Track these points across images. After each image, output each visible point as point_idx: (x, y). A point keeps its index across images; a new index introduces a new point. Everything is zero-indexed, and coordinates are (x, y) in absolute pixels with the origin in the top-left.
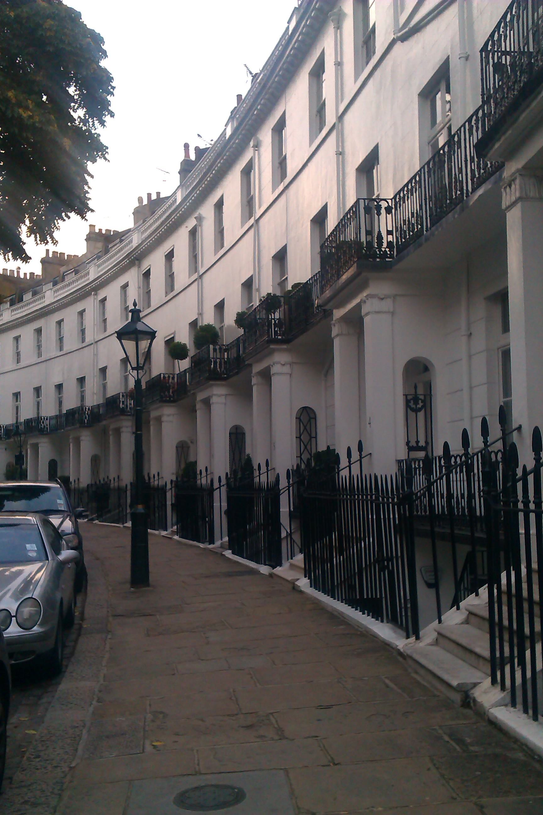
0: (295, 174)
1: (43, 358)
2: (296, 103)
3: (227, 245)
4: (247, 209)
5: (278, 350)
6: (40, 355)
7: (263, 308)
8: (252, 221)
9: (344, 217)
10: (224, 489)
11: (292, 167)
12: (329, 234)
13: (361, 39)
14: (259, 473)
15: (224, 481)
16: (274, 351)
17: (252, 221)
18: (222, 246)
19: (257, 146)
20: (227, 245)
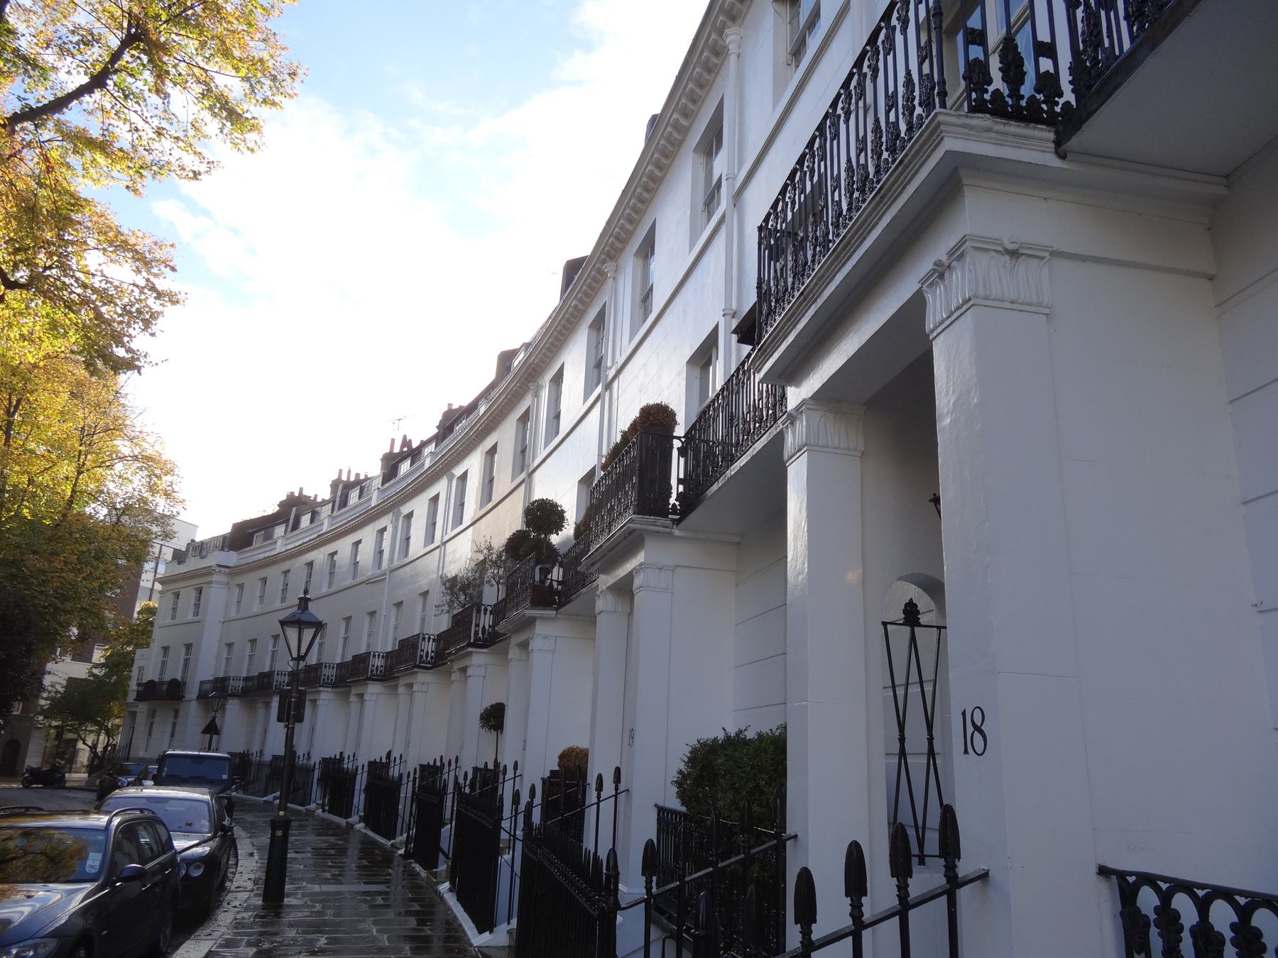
0: (666, 314)
1: (177, 621)
2: (574, 361)
3: (495, 499)
4: (519, 458)
5: (542, 618)
6: (173, 617)
7: (110, 873)
8: (523, 475)
9: (737, 371)
10: (365, 775)
11: (565, 424)
12: (718, 388)
13: (593, 363)
14: (599, 796)
15: (366, 768)
16: (470, 654)
17: (523, 475)
18: (490, 500)
19: (537, 395)
20: (495, 499)
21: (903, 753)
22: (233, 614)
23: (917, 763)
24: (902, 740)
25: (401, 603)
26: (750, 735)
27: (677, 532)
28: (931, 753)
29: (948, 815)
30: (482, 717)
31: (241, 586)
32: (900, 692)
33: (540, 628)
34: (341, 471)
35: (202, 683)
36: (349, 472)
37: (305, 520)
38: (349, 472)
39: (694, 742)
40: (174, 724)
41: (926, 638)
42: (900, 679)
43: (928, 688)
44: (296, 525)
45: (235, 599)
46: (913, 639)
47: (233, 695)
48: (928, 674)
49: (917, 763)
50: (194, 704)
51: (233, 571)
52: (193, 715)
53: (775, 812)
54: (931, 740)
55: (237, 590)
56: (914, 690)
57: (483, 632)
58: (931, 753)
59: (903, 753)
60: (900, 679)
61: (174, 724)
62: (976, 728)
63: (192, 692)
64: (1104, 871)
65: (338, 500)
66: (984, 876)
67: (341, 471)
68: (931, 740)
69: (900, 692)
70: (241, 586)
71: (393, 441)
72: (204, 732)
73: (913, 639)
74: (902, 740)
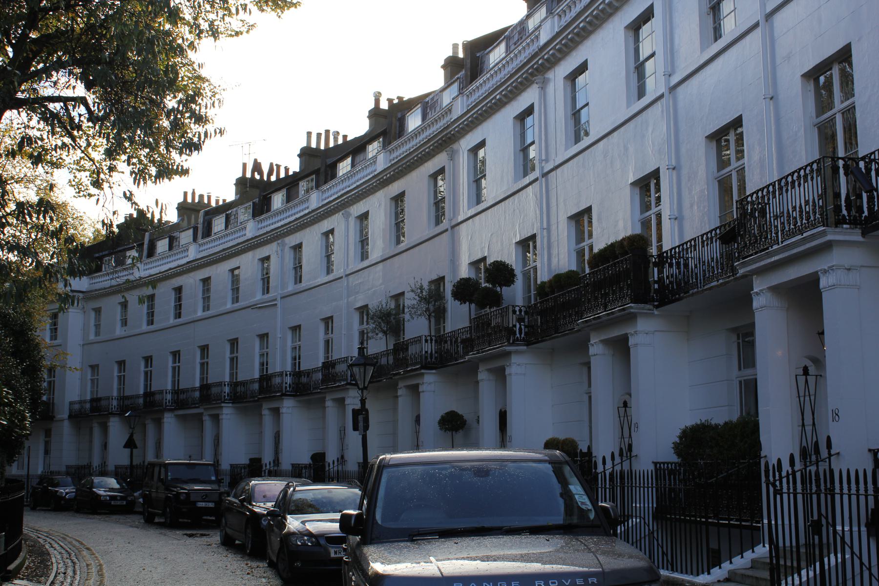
5: (517, 352)
16: (423, 374)
21: (803, 425)
22: (92, 337)
23: (809, 429)
24: (803, 419)
25: (299, 327)
26: (713, 423)
27: (656, 312)
28: (814, 424)
29: (829, 438)
30: (439, 423)
31: (98, 311)
32: (802, 399)
33: (514, 359)
34: (185, 194)
35: (71, 403)
36: (193, 193)
37: (162, 245)
38: (193, 193)
39: (683, 427)
40: (47, 444)
41: (812, 380)
42: (802, 394)
43: (812, 398)
44: (151, 252)
45: (92, 322)
46: (806, 381)
47: (112, 414)
48: (812, 392)
49: (809, 429)
50: (66, 423)
51: (90, 296)
52: (117, 431)
53: (757, 445)
54: (814, 419)
55: (93, 314)
56: (807, 398)
57: (431, 358)
58: (814, 424)
59: (803, 425)
60: (802, 394)
61: (47, 444)
62: (836, 414)
63: (63, 413)
64: (870, 450)
65: (200, 226)
66: (838, 454)
67: (185, 194)
68: (814, 419)
69: (802, 399)
70: (98, 311)
71: (245, 165)
72: (125, 447)
73: (806, 381)
74: (803, 419)
